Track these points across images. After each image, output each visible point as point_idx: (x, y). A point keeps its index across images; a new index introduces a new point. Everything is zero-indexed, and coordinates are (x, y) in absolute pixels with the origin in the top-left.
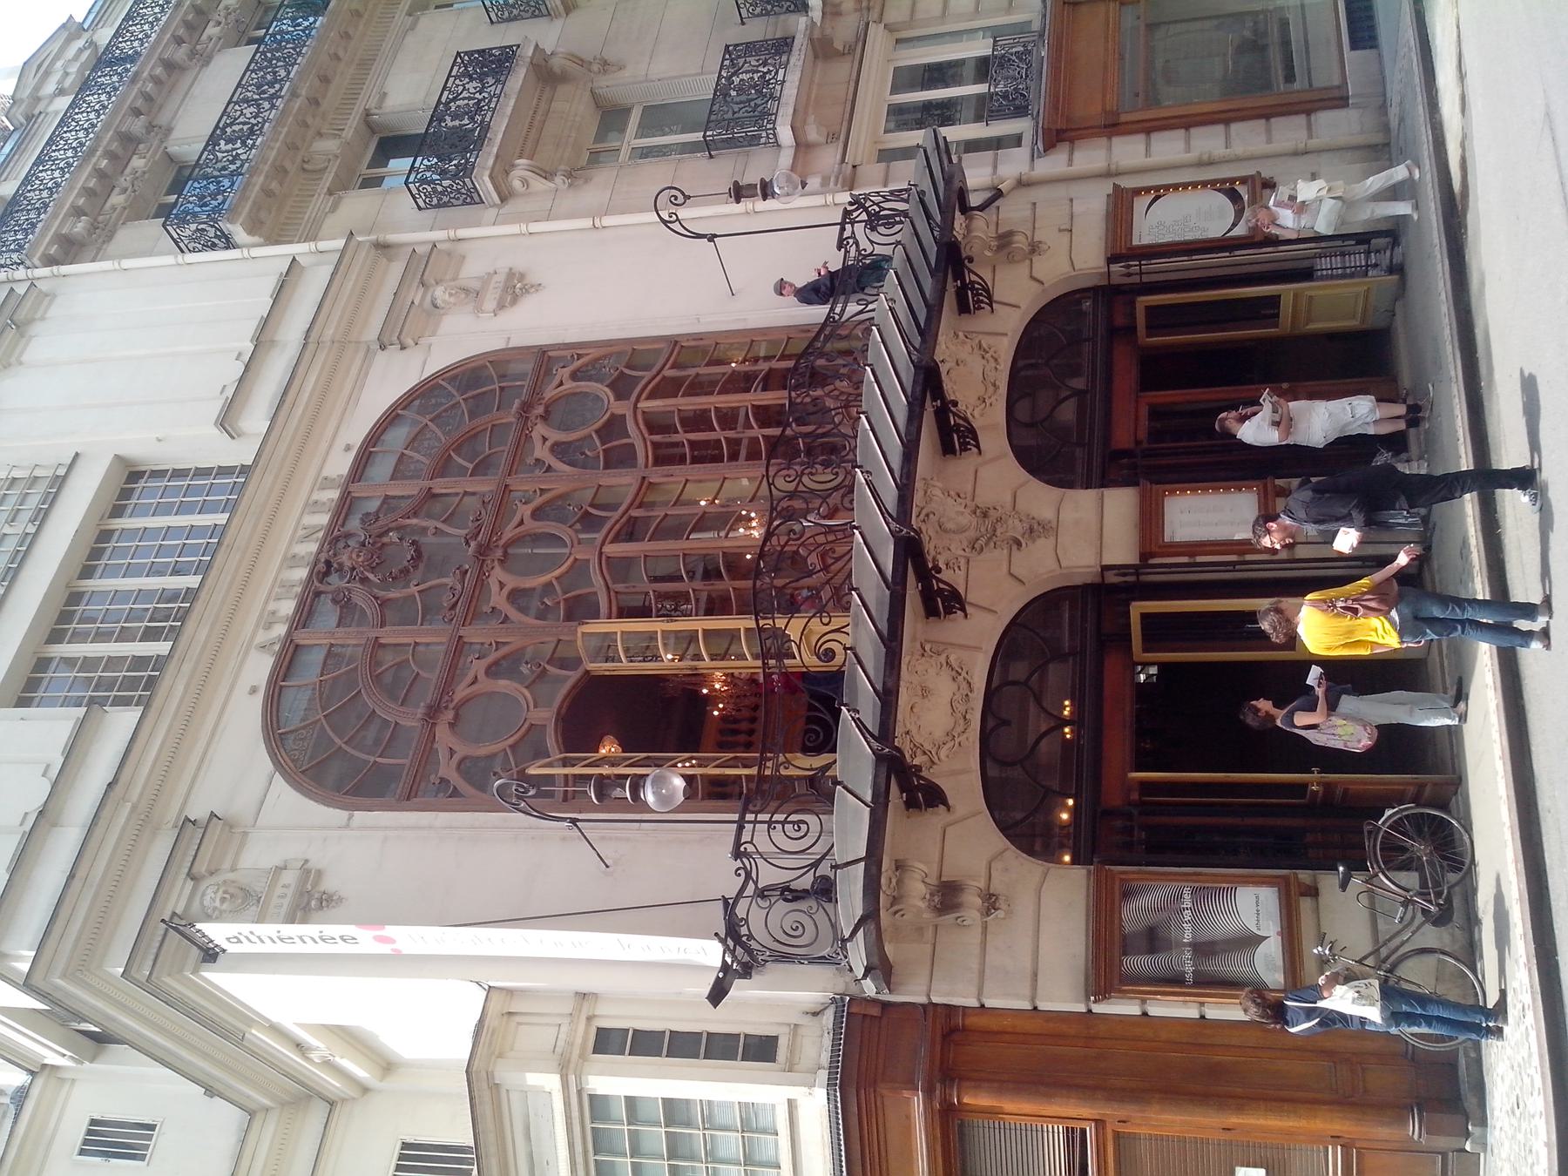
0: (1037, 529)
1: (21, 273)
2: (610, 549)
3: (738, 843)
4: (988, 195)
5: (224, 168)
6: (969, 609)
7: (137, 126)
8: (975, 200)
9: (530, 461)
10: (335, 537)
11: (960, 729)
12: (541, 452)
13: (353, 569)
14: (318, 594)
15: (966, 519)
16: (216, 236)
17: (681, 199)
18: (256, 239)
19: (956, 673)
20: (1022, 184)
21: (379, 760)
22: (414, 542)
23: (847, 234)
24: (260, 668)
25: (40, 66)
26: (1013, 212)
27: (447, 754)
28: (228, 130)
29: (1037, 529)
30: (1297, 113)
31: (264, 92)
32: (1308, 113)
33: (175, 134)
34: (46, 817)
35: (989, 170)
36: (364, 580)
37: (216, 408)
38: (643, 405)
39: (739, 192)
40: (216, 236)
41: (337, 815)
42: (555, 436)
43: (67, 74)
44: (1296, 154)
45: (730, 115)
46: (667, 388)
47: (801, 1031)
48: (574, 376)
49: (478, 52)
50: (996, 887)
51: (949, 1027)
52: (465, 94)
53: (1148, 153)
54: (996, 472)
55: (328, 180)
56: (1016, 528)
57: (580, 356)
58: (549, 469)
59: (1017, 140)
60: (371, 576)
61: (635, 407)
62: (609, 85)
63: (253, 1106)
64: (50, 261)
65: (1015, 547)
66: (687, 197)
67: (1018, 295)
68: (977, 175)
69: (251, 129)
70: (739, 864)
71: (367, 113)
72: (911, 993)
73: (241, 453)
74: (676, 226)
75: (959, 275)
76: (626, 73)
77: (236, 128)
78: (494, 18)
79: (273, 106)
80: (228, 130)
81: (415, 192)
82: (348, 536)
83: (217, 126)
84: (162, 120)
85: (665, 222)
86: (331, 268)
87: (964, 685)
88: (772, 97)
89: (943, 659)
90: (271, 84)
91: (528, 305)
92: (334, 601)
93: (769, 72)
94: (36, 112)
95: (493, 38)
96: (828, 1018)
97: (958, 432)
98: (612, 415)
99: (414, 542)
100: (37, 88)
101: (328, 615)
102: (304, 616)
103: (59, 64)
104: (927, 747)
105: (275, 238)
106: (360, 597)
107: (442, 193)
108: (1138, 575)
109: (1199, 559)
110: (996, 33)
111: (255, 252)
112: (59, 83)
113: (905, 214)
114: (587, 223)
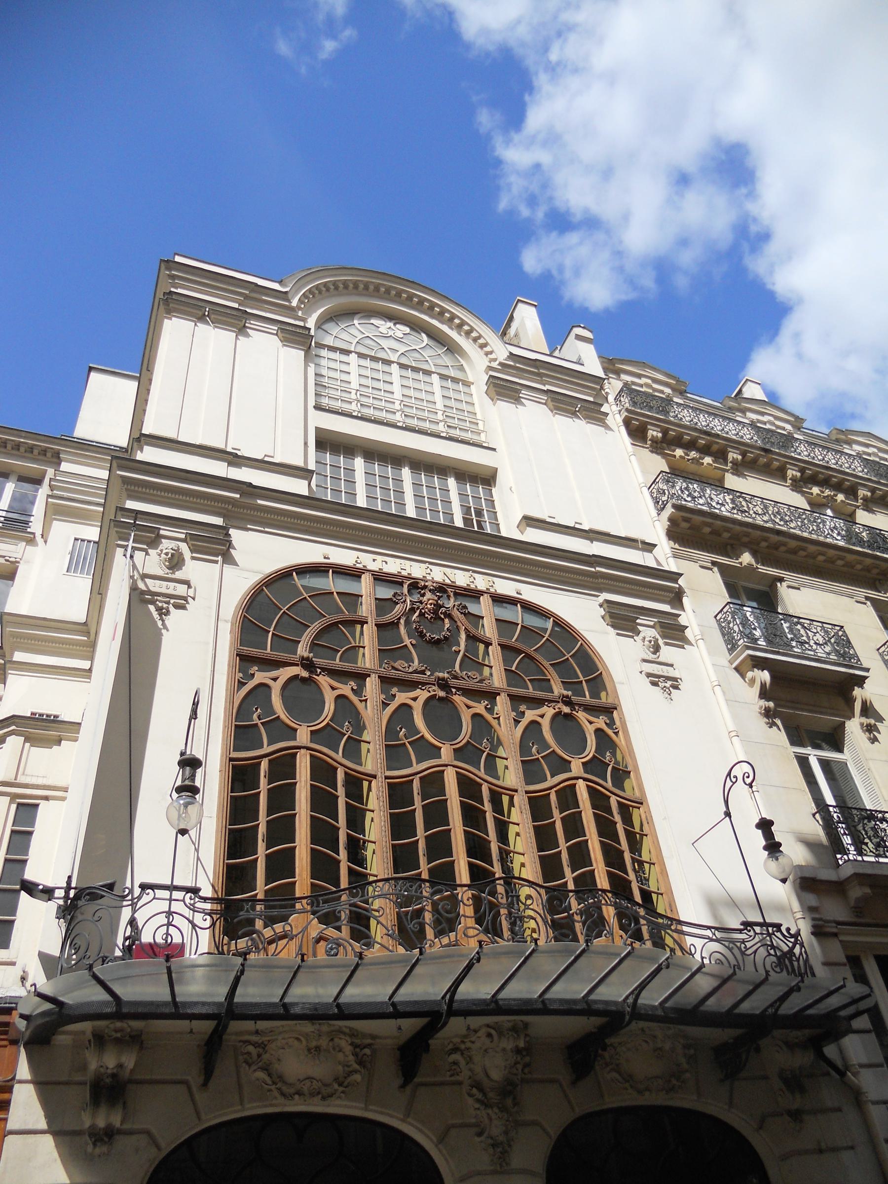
3: (153, 887)
4: (839, 1063)
5: (712, 499)
8: (830, 1051)
11: (285, 1089)
17: (748, 781)
21: (270, 634)
35: (864, 1060)
36: (413, 610)
42: (545, 724)
46: (599, 799)
48: (598, 731)
50: (122, 1143)
52: (810, 634)
57: (616, 733)
58: (517, 722)
61: (577, 778)
66: (751, 785)
69: (746, 511)
74: (729, 784)
81: (725, 610)
85: (729, 774)
98: (570, 762)
104: (265, 1057)
105: (672, 534)
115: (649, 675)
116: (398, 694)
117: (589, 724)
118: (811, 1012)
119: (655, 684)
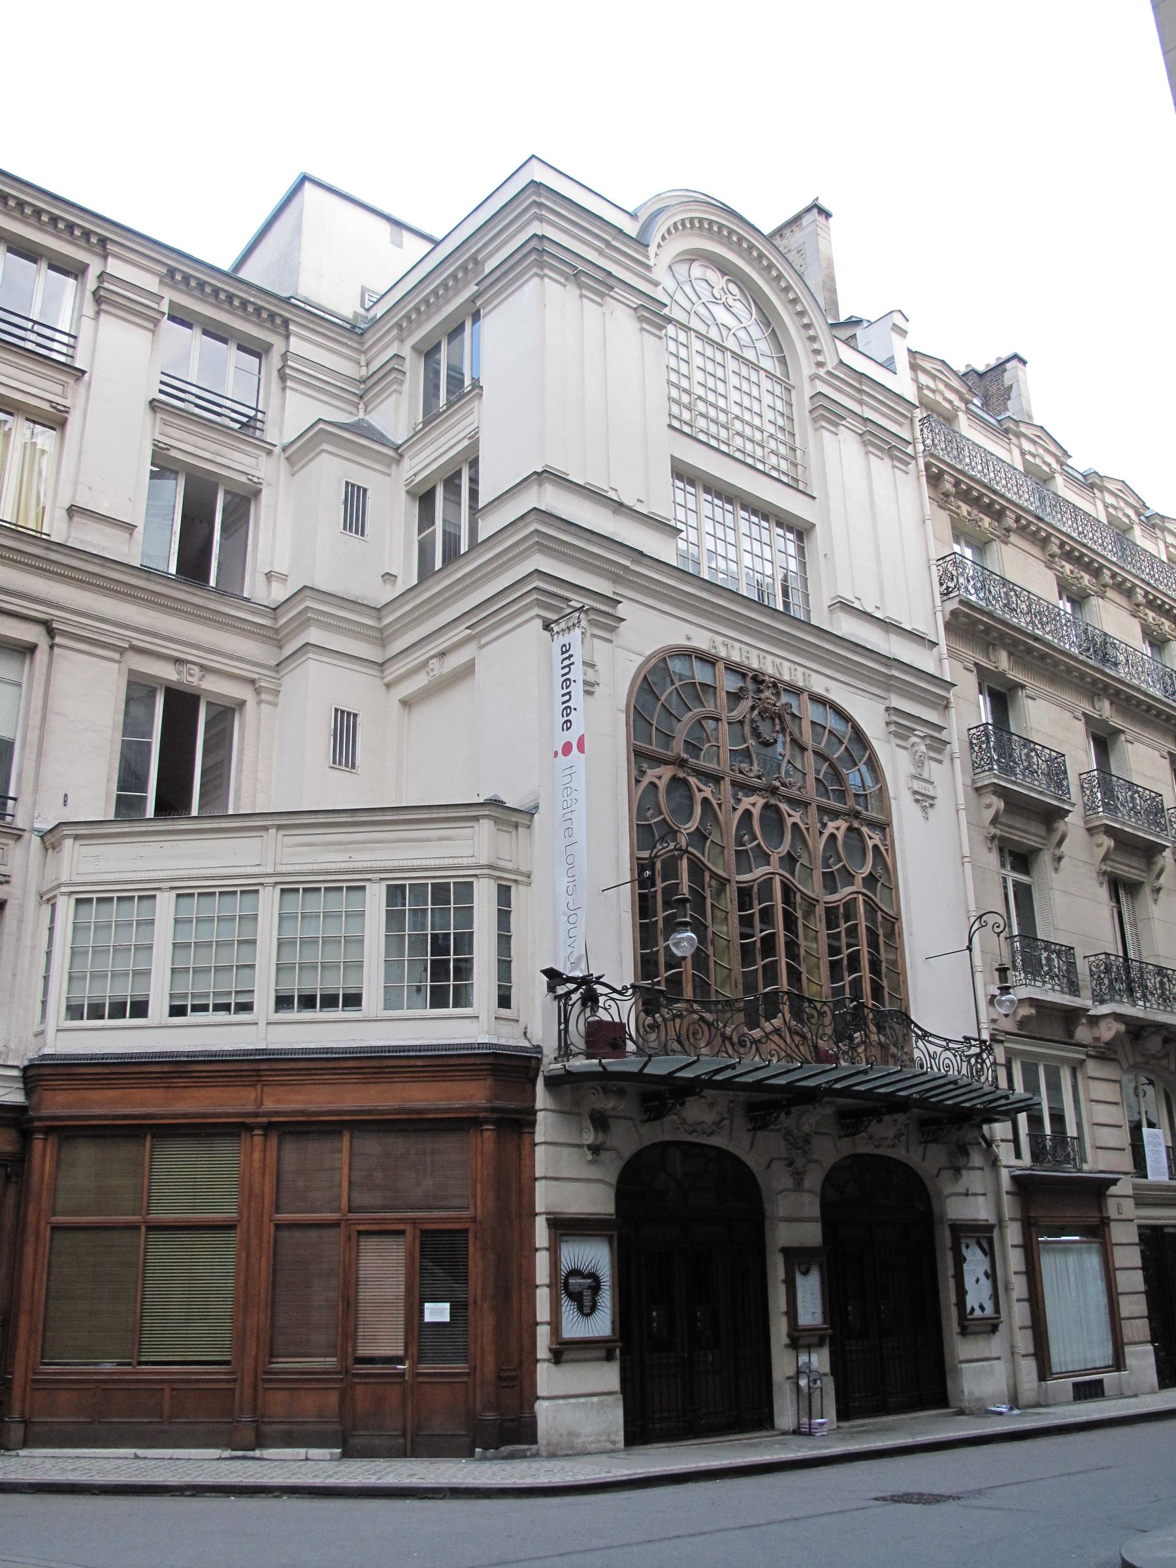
0: (799, 1178)
1: (921, 448)
2: (777, 879)
5: (990, 592)
7: (1010, 521)
8: (985, 1127)
9: (825, 819)
10: (776, 686)
12: (831, 826)
14: (744, 676)
15: (806, 1129)
16: (948, 588)
18: (948, 617)
19: (717, 1124)
22: (1005, 990)
23: (973, 1042)
24: (702, 641)
25: (1038, 437)
28: (1012, 593)
29: (799, 1178)
30: (1035, 1347)
32: (1035, 1355)
33: (1003, 546)
34: (619, 507)
37: (848, 596)
38: (861, 897)
40: (948, 588)
41: (623, 705)
42: (840, 835)
44: (1012, 1347)
47: (514, 1024)
48: (875, 847)
51: (517, 1124)
53: (1013, 1246)
54: (828, 1151)
55: (984, 663)
56: (800, 1163)
59: (1018, 1155)
60: (756, 712)
61: (858, 893)
62: (1046, 858)
63: (384, 612)
64: (928, 466)
67: (925, 1160)
71: (1023, 687)
72: (542, 1097)
76: (1053, 874)
79: (1028, 624)
82: (778, 694)
84: (1013, 538)
86: (931, 671)
89: (726, 1115)
90: (1041, 622)
91: (916, 808)
92: (741, 689)
94: (1011, 436)
96: (525, 1043)
99: (776, 741)
100: (1026, 437)
101: (731, 684)
102: (734, 669)
103: (1041, 451)
106: (745, 705)
107: (980, 747)
110: (1080, 1138)
111: (939, 615)
114: (967, 852)
115: (915, 792)
116: (744, 799)
117: (873, 839)
118: (738, 1079)
119: (917, 801)
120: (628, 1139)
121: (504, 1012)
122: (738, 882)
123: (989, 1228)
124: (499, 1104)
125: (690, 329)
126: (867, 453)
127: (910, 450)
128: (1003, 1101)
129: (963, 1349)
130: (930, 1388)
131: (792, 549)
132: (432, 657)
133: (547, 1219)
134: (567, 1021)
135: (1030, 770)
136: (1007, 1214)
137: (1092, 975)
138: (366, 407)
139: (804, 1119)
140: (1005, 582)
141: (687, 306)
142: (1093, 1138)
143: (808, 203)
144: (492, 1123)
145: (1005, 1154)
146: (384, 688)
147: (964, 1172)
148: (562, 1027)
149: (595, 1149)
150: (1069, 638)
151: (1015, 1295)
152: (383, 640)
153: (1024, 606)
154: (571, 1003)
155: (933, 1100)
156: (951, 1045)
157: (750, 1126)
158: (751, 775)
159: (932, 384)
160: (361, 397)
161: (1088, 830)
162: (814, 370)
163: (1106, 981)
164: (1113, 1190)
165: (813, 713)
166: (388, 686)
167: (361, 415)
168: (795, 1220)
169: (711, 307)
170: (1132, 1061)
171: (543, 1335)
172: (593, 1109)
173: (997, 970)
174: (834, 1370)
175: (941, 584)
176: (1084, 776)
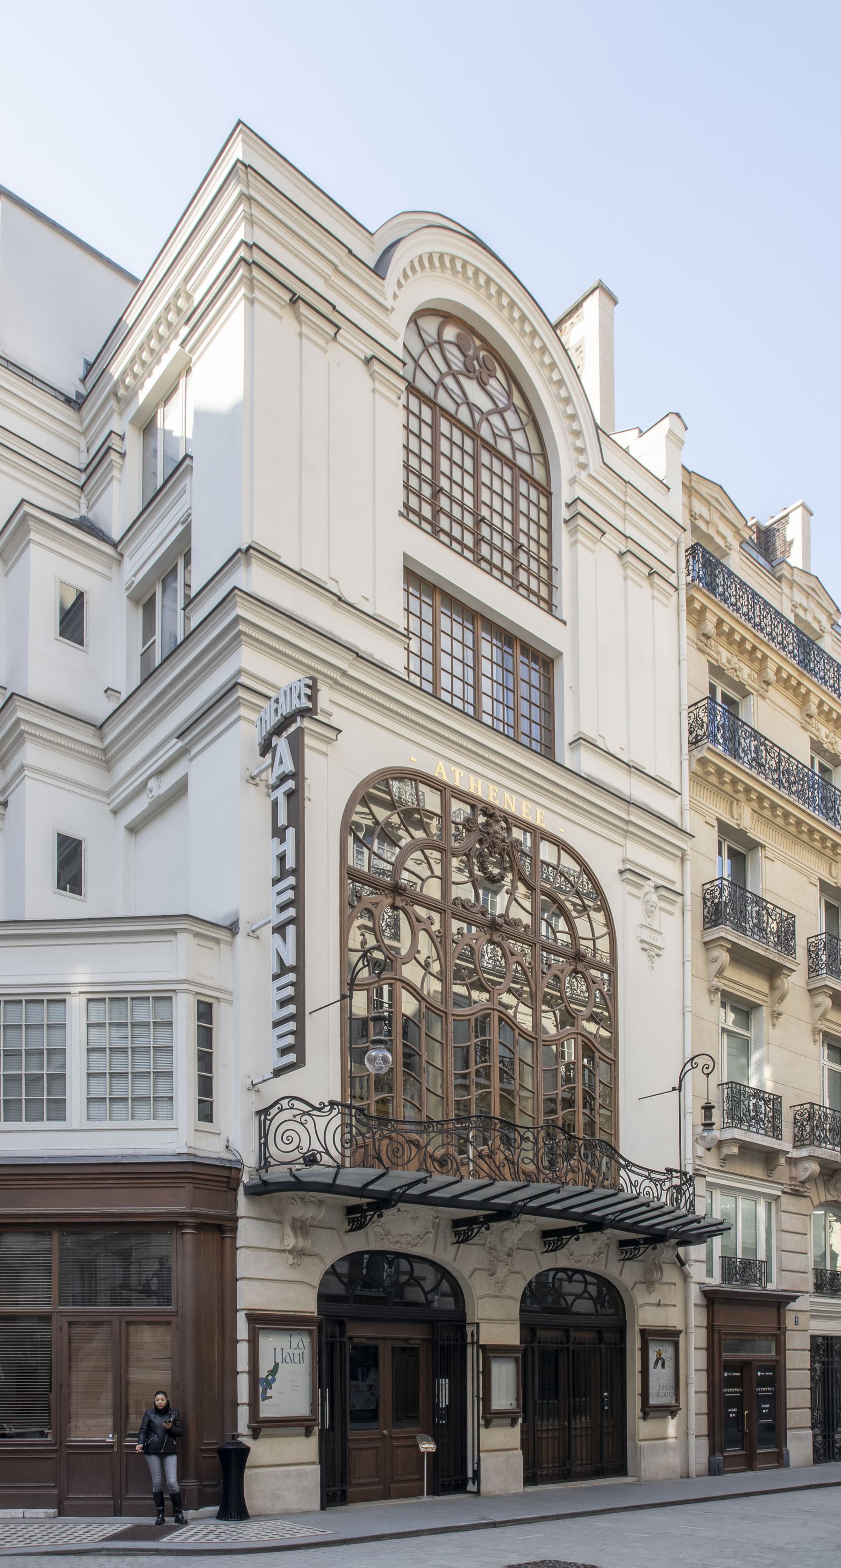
5: (740, 743)
6: (457, 1245)
13: (488, 834)
16: (697, 735)
17: (706, 1071)
20: (686, 1277)
23: (674, 1174)
25: (813, 590)
26: (670, 1274)
27: (374, 901)
31: (784, 775)
39: (708, 1109)
40: (697, 735)
43: (805, 610)
45: (742, 1098)
49: (794, 930)
51: (222, 1229)
54: (535, 1263)
59: (710, 1273)
63: (106, 729)
64: (690, 600)
65: (489, 1272)
67: (625, 1275)
68: (696, 1252)
70: (327, 1104)
71: (763, 846)
72: (243, 1205)
73: (566, 756)
74: (689, 1066)
75: (646, 1241)
77: (764, 754)
78: (811, 940)
80: (763, 748)
83: (766, 739)
87: (415, 1242)
88: (750, 1126)
90: (788, 781)
93: (764, 1124)
95: (801, 943)
97: (558, 1240)
108: (473, 1343)
109: (481, 1376)
110: (767, 1263)
112: (801, 605)
113: (678, 1208)
115: (642, 941)
119: (644, 949)
120: (335, 1246)
121: (205, 1126)
122: (454, 1015)
123: (677, 1333)
124: (195, 1210)
125: (436, 404)
126: (626, 578)
127: (673, 579)
128: (695, 1225)
129: (641, 1429)
130: (610, 1457)
131: (535, 679)
132: (150, 777)
133: (246, 1314)
134: (266, 1136)
135: (760, 929)
136: (693, 1322)
137: (795, 1123)
138: (88, 501)
139: (506, 1235)
140: (756, 735)
141: (435, 377)
142: (780, 1262)
143: (593, 283)
144: (193, 1227)
145: (697, 1272)
146: (111, 815)
147: (657, 1286)
148: (263, 1140)
149: (298, 1253)
150: (814, 801)
151: (693, 1388)
152: (107, 762)
153: (773, 762)
154: (269, 1118)
155: (629, 1221)
156: (652, 1175)
157: (455, 1240)
158: (474, 910)
159: (706, 514)
160: (82, 488)
161: (809, 990)
162: (576, 470)
163: (808, 1128)
164: (792, 1306)
165: (547, 852)
166: (115, 812)
167: (83, 512)
168: (496, 1321)
169: (463, 380)
170: (823, 1200)
171: (243, 1415)
172: (294, 1219)
173: (703, 1108)
174: (524, 1445)
175: (691, 733)
176: (813, 940)
